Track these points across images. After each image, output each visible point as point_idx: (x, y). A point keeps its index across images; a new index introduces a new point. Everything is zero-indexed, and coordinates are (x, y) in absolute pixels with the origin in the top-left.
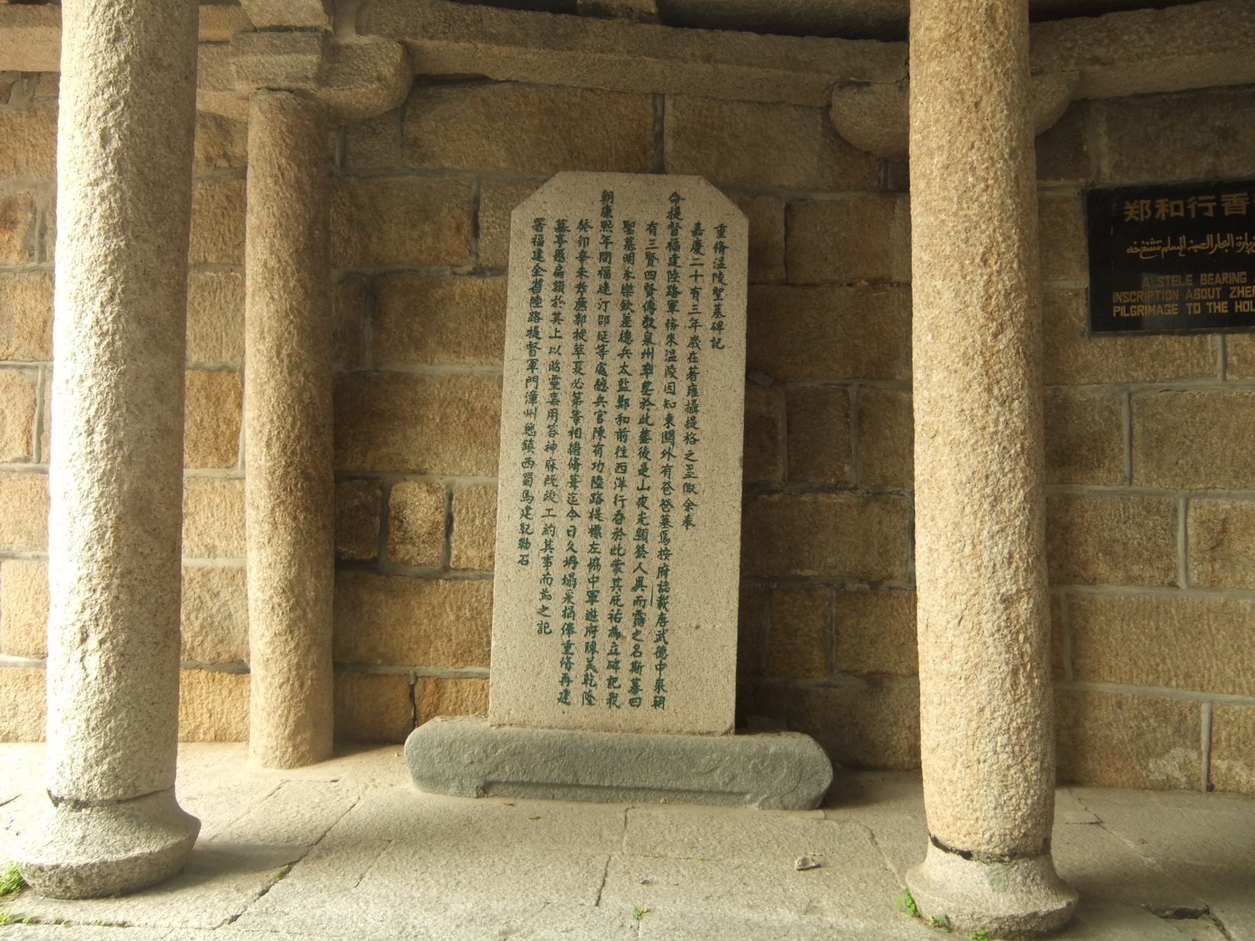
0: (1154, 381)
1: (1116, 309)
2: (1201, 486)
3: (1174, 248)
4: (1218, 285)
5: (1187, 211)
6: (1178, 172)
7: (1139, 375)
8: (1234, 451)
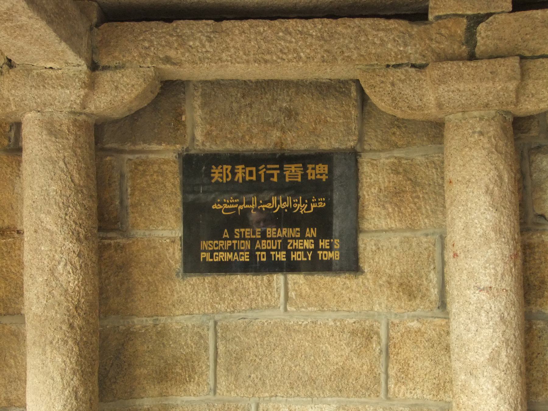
0: (234, 312)
1: (203, 255)
2: (267, 394)
3: (247, 206)
4: (279, 238)
5: (258, 177)
6: (254, 142)
7: (222, 307)
8: (291, 367)
